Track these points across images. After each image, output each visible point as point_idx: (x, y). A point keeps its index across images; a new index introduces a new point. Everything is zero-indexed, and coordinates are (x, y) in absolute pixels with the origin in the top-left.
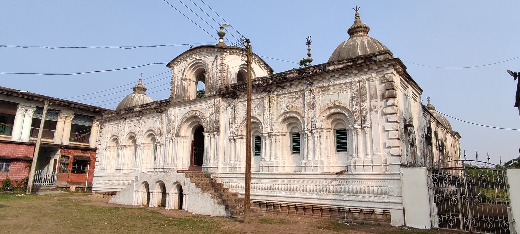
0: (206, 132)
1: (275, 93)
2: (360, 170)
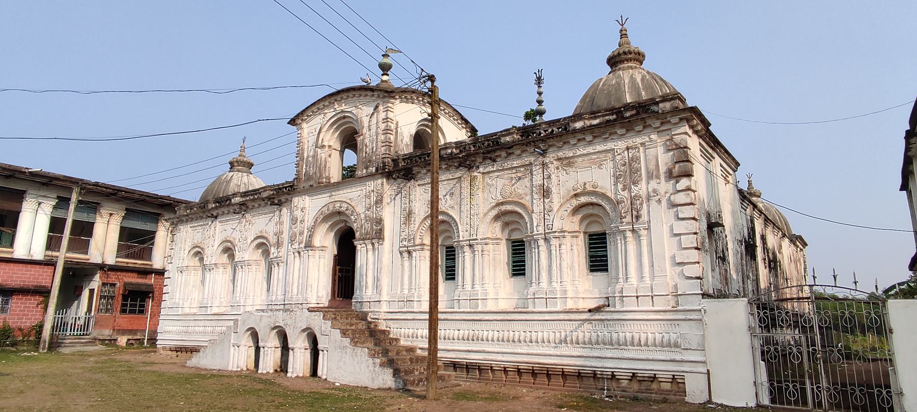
0: (360, 240)
1: (481, 170)
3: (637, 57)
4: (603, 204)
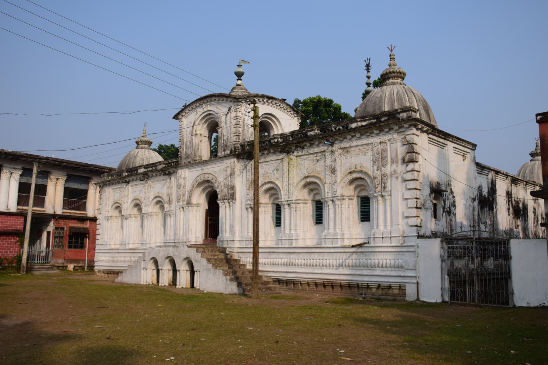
0: (221, 200)
1: (295, 154)
2: (379, 243)
3: (399, 75)
4: (366, 178)
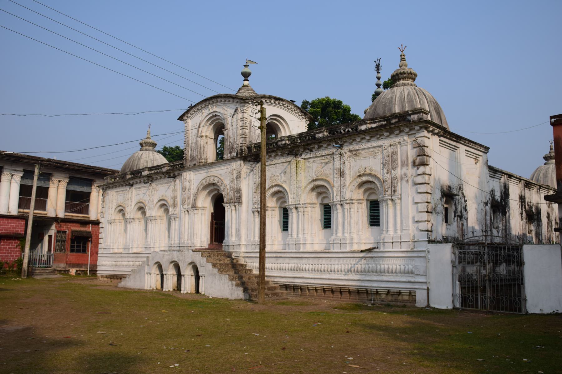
0: (227, 203)
1: (303, 156)
3: (410, 76)
4: (375, 182)
